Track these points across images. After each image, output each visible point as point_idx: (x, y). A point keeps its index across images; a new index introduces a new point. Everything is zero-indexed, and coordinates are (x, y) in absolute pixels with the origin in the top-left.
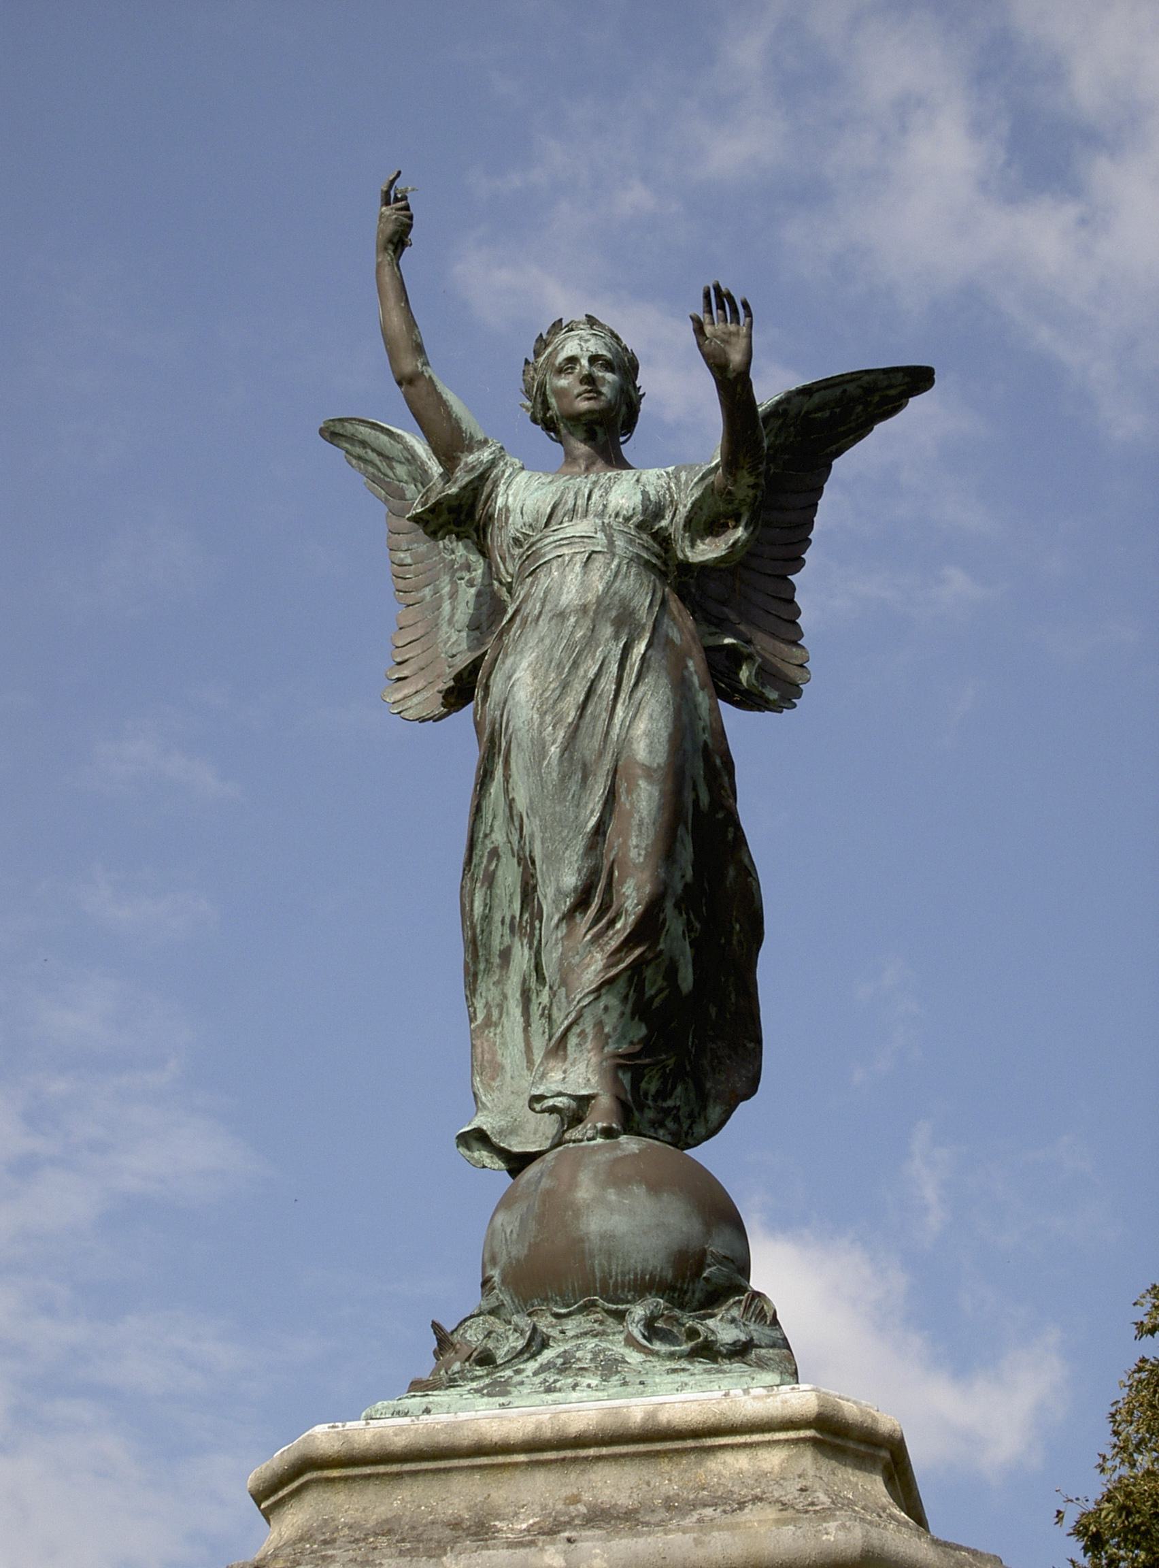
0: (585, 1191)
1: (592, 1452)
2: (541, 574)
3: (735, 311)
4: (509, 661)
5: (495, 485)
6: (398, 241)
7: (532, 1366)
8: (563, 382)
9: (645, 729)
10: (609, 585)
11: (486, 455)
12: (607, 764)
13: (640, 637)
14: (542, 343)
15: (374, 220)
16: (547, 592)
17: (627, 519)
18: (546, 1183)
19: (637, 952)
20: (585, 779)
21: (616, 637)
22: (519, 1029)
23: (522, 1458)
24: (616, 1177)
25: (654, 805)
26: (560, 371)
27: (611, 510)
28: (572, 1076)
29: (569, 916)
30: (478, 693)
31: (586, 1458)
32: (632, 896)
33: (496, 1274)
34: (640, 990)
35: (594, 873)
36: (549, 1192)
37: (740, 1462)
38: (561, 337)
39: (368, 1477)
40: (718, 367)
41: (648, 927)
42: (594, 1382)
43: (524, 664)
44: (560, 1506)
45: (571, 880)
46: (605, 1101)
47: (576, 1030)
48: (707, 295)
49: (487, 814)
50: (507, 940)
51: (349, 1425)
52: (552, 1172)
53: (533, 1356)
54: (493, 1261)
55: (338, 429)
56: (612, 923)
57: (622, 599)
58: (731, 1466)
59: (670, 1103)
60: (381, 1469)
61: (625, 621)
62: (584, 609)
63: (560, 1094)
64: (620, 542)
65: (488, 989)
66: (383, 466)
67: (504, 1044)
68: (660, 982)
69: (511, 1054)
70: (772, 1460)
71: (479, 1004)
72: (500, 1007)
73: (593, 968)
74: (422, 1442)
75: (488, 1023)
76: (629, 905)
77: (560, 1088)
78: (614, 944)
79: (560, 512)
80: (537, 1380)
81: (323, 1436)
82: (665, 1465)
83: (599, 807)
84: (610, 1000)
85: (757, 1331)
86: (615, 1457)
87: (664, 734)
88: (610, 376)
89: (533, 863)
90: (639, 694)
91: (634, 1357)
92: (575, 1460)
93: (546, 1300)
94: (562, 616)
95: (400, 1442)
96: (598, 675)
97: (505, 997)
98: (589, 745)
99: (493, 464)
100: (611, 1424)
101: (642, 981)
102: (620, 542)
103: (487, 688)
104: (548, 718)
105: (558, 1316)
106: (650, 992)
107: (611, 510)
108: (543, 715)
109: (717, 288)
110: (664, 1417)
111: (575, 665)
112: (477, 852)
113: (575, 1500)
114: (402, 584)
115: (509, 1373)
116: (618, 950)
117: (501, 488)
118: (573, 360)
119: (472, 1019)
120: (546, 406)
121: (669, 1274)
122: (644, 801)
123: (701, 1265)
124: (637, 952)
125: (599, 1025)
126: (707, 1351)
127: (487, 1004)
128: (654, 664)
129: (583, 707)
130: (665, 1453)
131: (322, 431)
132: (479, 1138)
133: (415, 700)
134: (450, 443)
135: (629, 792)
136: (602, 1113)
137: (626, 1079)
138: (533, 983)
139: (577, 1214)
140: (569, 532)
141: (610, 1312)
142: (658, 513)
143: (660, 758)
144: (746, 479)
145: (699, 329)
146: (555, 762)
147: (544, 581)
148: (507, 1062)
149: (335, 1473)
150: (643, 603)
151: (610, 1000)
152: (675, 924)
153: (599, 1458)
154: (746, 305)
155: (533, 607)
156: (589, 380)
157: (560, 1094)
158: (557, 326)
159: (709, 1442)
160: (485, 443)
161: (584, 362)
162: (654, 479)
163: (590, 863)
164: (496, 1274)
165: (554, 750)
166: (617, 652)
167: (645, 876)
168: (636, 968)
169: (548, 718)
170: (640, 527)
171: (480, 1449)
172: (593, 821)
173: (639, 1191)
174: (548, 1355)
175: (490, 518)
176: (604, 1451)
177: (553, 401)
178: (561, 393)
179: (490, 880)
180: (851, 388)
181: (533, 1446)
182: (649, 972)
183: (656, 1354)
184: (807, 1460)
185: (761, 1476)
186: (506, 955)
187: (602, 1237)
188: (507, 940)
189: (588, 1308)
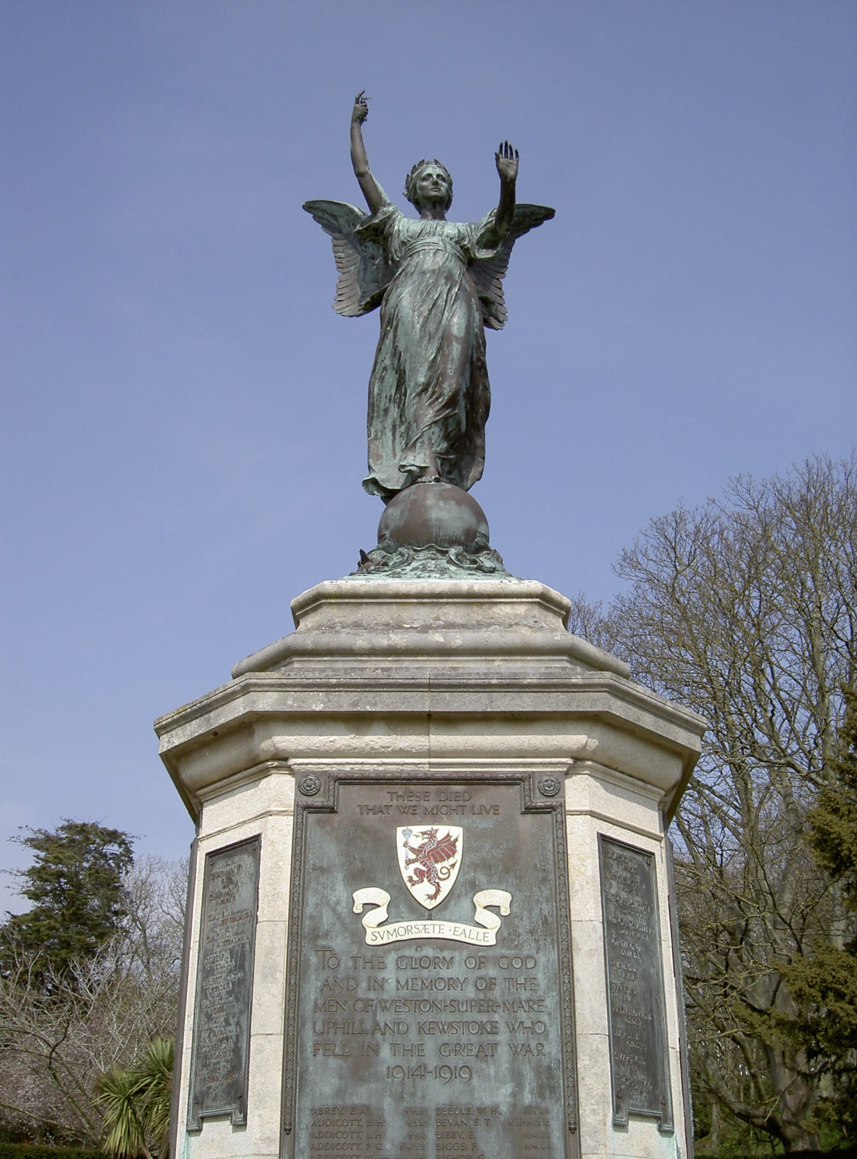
0: (430, 501)
1: (445, 600)
2: (415, 256)
3: (511, 154)
4: (399, 290)
5: (394, 220)
6: (360, 118)
7: (408, 568)
8: (425, 184)
9: (457, 321)
10: (444, 264)
11: (391, 209)
12: (440, 334)
13: (455, 286)
14: (415, 168)
15: (348, 111)
16: (417, 263)
17: (451, 239)
18: (412, 497)
19: (447, 412)
20: (430, 339)
21: (446, 284)
22: (390, 441)
23: (415, 600)
24: (443, 497)
25: (459, 352)
26: (424, 179)
27: (445, 234)
28: (418, 459)
29: (419, 394)
30: (383, 302)
31: (442, 603)
32: (448, 389)
33: (387, 533)
34: (446, 428)
35: (431, 378)
36: (414, 501)
37: (507, 609)
38: (425, 166)
39: (347, 603)
40: (503, 175)
41: (452, 402)
42: (438, 576)
43: (406, 291)
44: (431, 621)
45: (422, 379)
46: (432, 469)
47: (420, 440)
48: (501, 146)
49: (383, 352)
50: (387, 405)
51: (339, 582)
52: (415, 493)
53: (409, 565)
54: (387, 528)
55: (312, 206)
56: (437, 399)
57: (449, 269)
58: (503, 611)
59: (451, 476)
60: (353, 601)
61: (449, 277)
62: (434, 271)
63: (413, 465)
64: (449, 247)
65: (376, 423)
66: (333, 220)
67: (383, 447)
68: (454, 426)
69: (386, 452)
70: (521, 610)
71: (373, 430)
72: (382, 432)
73: (429, 415)
74: (372, 590)
75: (376, 438)
76: (446, 392)
77: (413, 463)
78: (437, 407)
79: (424, 232)
80: (413, 573)
81: (328, 586)
82: (475, 608)
83: (435, 351)
84: (436, 429)
85: (498, 566)
86: (454, 603)
87: (464, 325)
88: (444, 184)
89: (405, 372)
90: (454, 308)
91: (453, 568)
92: (437, 603)
93: (410, 544)
94: (424, 273)
95: (363, 590)
96: (438, 298)
97: (385, 428)
98: (432, 327)
99: (393, 213)
100: (453, 589)
101: (447, 424)
102: (449, 247)
103: (387, 301)
104: (416, 313)
105: (416, 551)
106: (450, 429)
107: (445, 234)
108: (414, 312)
109: (506, 144)
110: (476, 588)
111: (428, 293)
112: (378, 367)
113: (437, 619)
114: (340, 265)
115: (399, 570)
116: (439, 410)
117: (397, 223)
118: (430, 175)
119: (369, 436)
120: (415, 192)
121: (463, 538)
122: (456, 350)
123: (475, 537)
124: (447, 412)
125: (430, 439)
126: (480, 569)
127: (376, 431)
128: (460, 297)
129: (430, 310)
130: (476, 603)
131: (303, 207)
132: (374, 482)
133: (348, 309)
134: (374, 203)
135: (448, 346)
136: (431, 476)
137: (439, 462)
138: (398, 423)
139: (427, 510)
140: (428, 241)
141: (438, 551)
142: (463, 239)
143: (462, 334)
144: (505, 226)
145: (497, 159)
146: (418, 331)
147: (416, 259)
148: (384, 454)
149: (333, 601)
150: (457, 272)
151: (436, 429)
152: (462, 402)
153: (447, 603)
154: (516, 152)
155: (411, 269)
156: (436, 183)
157: (413, 465)
158: (422, 163)
159: (495, 600)
160: (390, 205)
161: (435, 177)
162: (462, 227)
163: (430, 373)
164: (387, 533)
165: (418, 326)
166: (446, 290)
167: (454, 381)
168: (446, 419)
169: (416, 313)
170: (457, 242)
171: (397, 596)
172: (432, 357)
173: (453, 503)
174: (414, 564)
175: (391, 234)
176: (450, 600)
177: (418, 191)
178: (422, 188)
179: (382, 379)
180: (527, 210)
181: (420, 596)
182: (450, 421)
183: (462, 567)
184: (536, 611)
185: (516, 616)
186: (386, 411)
187: (437, 520)
188: (387, 405)
189: (428, 549)
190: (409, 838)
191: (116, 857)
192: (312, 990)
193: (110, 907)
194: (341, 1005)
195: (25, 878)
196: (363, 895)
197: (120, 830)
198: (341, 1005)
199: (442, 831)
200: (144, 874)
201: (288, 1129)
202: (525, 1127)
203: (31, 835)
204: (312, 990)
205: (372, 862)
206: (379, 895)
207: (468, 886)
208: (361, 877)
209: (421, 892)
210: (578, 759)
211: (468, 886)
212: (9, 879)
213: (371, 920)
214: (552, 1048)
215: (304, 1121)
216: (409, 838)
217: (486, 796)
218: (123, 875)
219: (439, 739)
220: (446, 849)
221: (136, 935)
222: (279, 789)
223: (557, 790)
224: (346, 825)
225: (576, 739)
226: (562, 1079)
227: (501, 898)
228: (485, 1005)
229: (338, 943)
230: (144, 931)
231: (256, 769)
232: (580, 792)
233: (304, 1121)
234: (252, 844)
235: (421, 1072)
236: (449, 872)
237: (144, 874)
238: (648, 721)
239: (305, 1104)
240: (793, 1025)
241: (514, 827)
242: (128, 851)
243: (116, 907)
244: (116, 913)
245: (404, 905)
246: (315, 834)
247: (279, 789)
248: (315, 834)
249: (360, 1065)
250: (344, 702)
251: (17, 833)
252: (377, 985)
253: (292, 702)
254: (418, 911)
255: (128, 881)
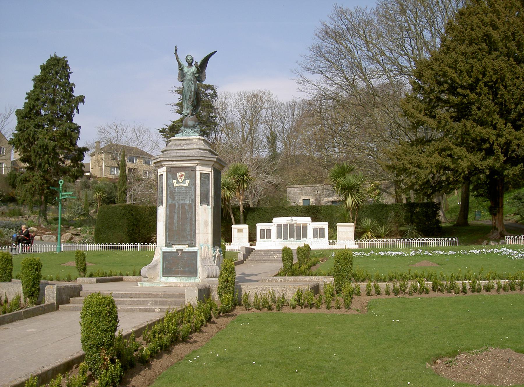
6: (176, 50)
32: (192, 100)
41: (193, 101)
190: (179, 174)
191: (210, 95)
192: (168, 192)
193: (210, 115)
194: (172, 192)
195: (176, 106)
196: (174, 181)
197: (211, 85)
198: (172, 192)
199: (182, 173)
200: (223, 100)
201: (166, 206)
202: (190, 205)
203: (176, 89)
204: (168, 192)
205: (175, 177)
206: (175, 181)
207: (185, 180)
208: (173, 179)
209: (180, 180)
210: (198, 164)
211: (185, 180)
212: (170, 107)
213: (175, 184)
214: (193, 197)
215: (168, 205)
216: (179, 174)
217: (187, 169)
218: (214, 102)
219: (181, 162)
220: (182, 175)
221: (222, 123)
222: (165, 168)
223: (196, 168)
224: (172, 172)
225: (197, 162)
226: (195, 201)
227: (188, 181)
228: (186, 193)
229: (171, 186)
230: (225, 122)
231: (162, 166)
232: (198, 168)
233: (168, 205)
234: (162, 175)
235: (180, 200)
236: (183, 178)
237: (223, 100)
238: (207, 159)
239: (168, 203)
240: (390, 166)
241: (190, 171)
242: (215, 92)
243: (212, 115)
244: (212, 117)
245: (178, 182)
246: (168, 174)
247: (165, 168)
248: (168, 174)
249: (174, 199)
250: (170, 159)
251: (171, 89)
252: (175, 191)
253: (165, 159)
254: (180, 183)
255: (216, 104)
